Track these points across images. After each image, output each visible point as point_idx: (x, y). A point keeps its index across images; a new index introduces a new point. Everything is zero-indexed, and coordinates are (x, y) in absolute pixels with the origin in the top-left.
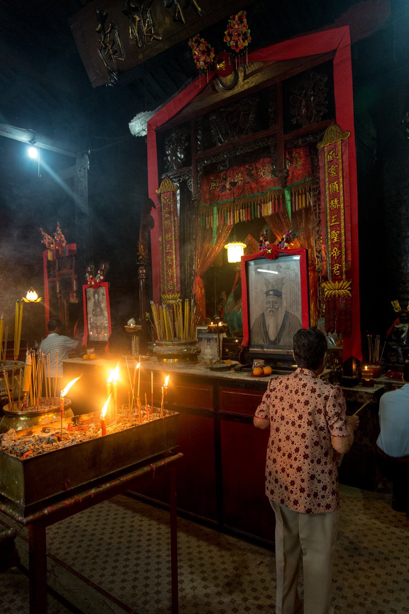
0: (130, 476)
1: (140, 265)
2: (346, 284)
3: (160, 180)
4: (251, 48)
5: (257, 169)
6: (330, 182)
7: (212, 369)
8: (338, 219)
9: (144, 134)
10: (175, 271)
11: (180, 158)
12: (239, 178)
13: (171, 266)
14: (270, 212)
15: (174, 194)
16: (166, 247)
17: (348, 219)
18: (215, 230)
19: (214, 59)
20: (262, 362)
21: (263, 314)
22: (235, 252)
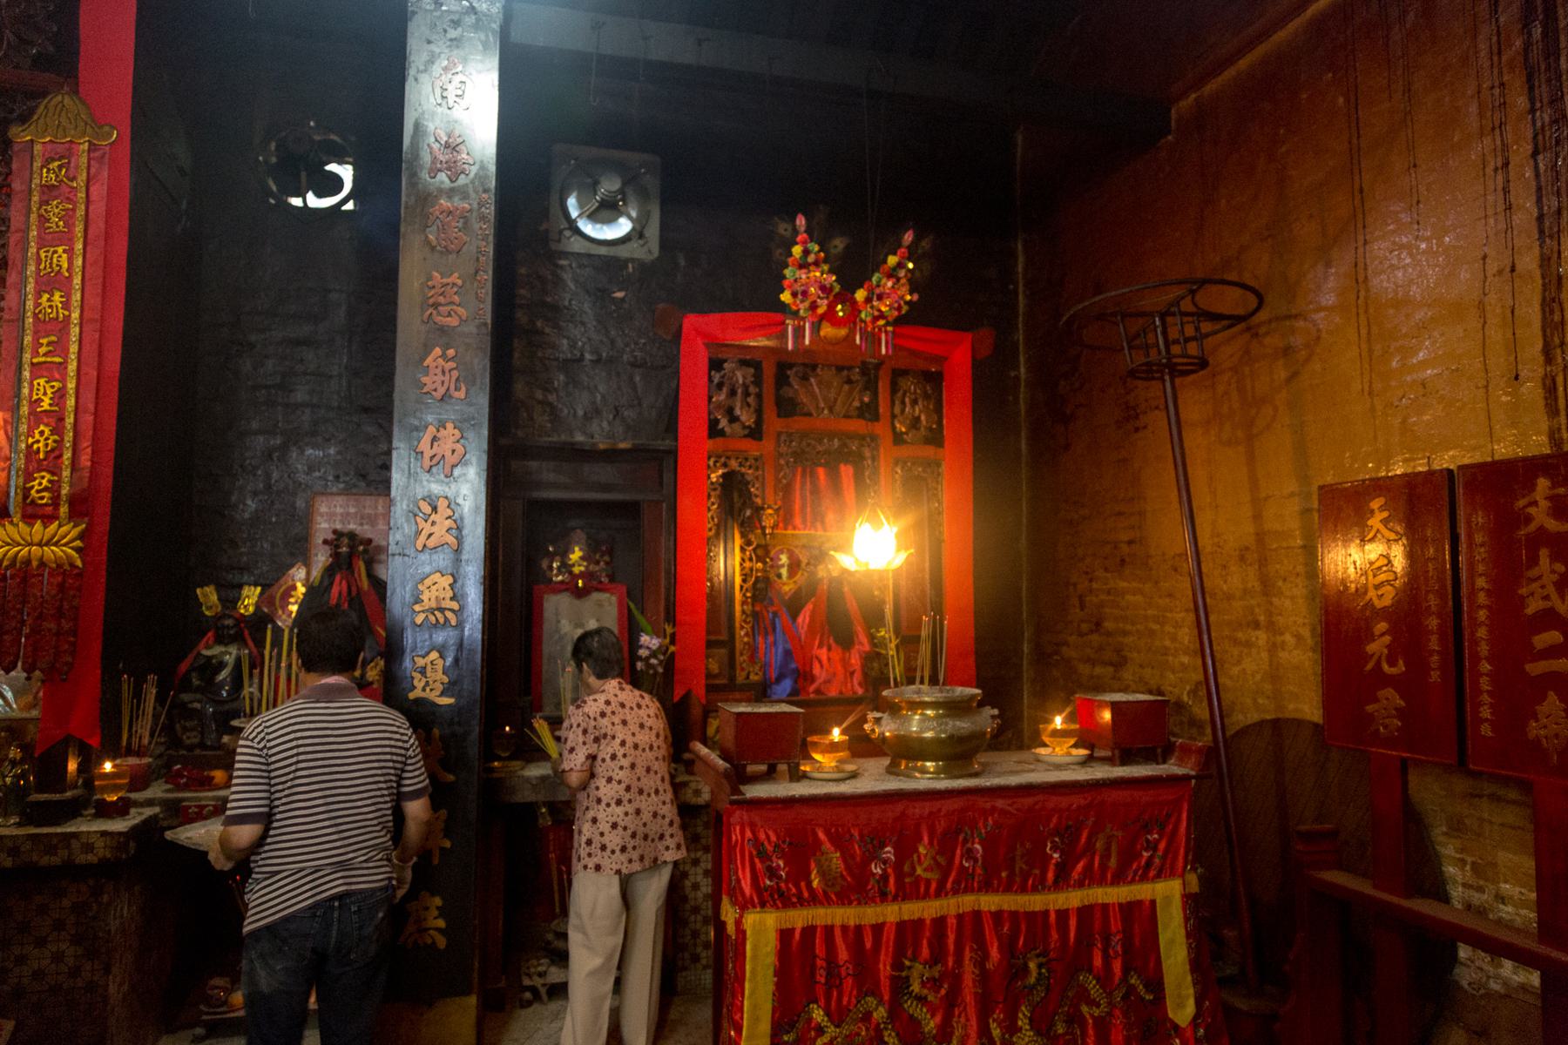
8: (60, 347)
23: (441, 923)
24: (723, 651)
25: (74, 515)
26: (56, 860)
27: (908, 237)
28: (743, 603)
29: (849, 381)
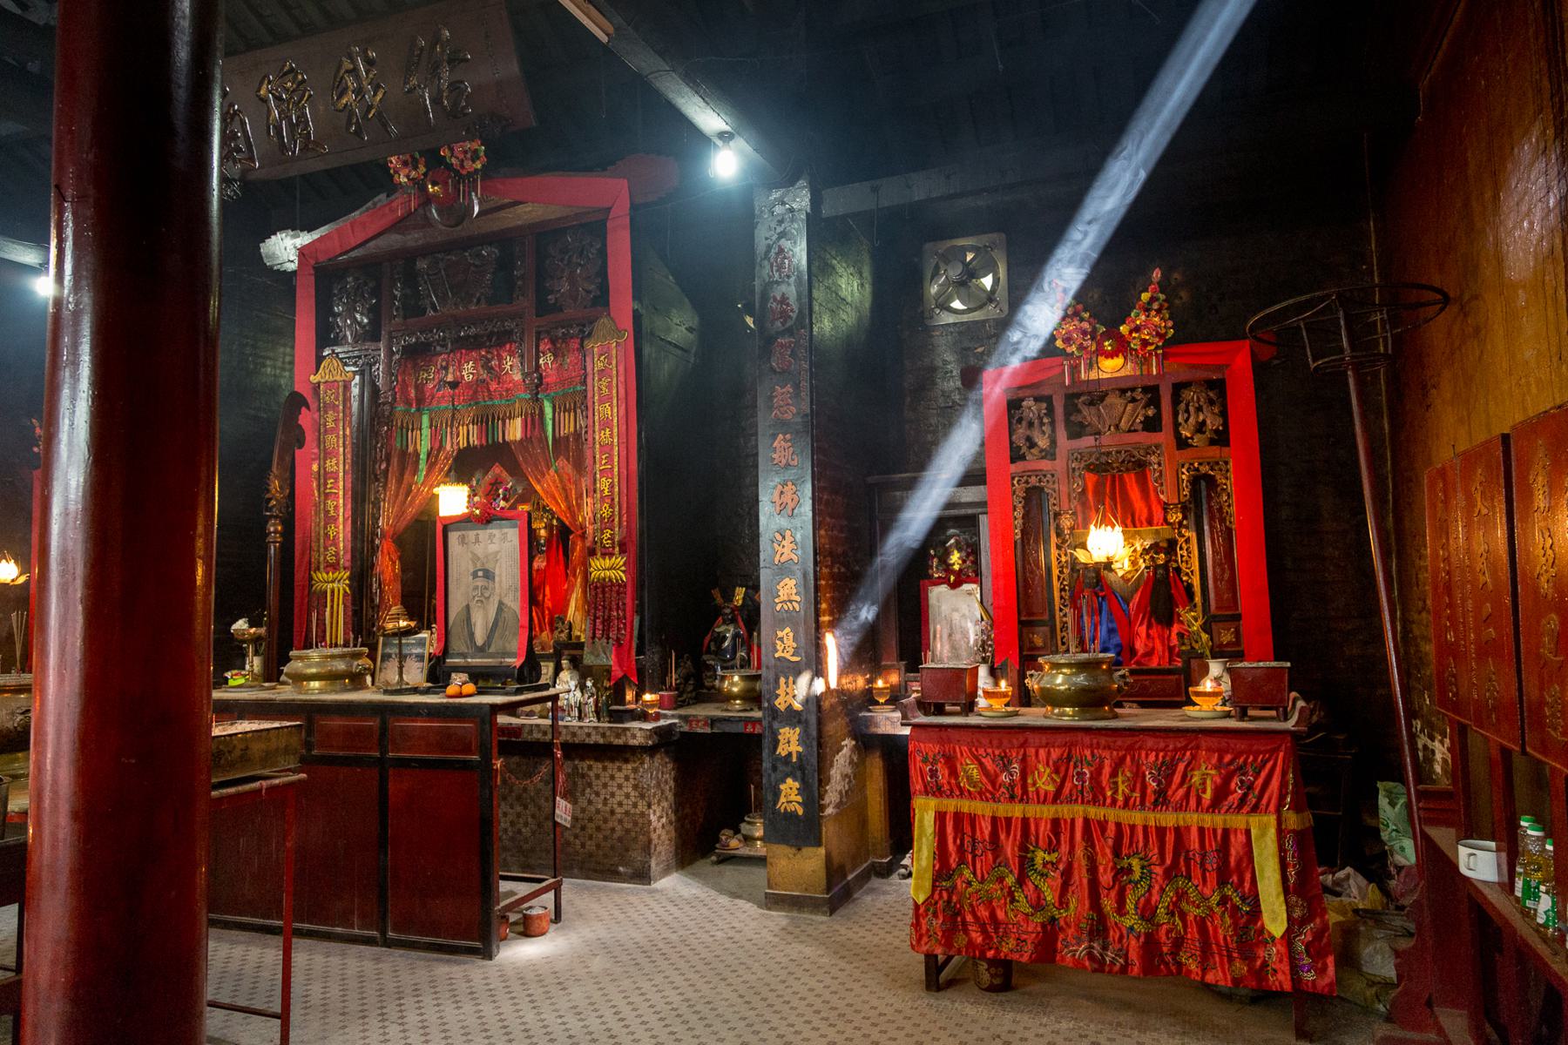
0: (232, 790)
1: (271, 517)
2: (619, 561)
3: (320, 359)
4: (486, 173)
5: (500, 358)
6: (601, 402)
7: (386, 692)
8: (610, 460)
9: (292, 267)
10: (341, 531)
11: (359, 324)
12: (469, 371)
13: (335, 519)
14: (519, 436)
15: (347, 387)
16: (326, 484)
17: (624, 464)
18: (423, 456)
19: (425, 175)
20: (464, 677)
21: (468, 607)
22: (453, 500)
23: (799, 799)
24: (1046, 629)
25: (622, 552)
26: (620, 742)
27: (1157, 274)
28: (1062, 590)
29: (1133, 400)
